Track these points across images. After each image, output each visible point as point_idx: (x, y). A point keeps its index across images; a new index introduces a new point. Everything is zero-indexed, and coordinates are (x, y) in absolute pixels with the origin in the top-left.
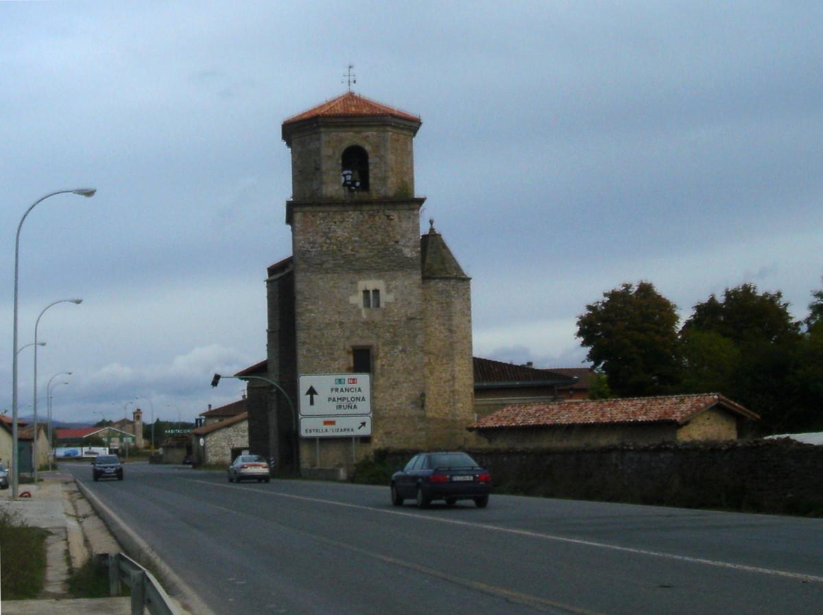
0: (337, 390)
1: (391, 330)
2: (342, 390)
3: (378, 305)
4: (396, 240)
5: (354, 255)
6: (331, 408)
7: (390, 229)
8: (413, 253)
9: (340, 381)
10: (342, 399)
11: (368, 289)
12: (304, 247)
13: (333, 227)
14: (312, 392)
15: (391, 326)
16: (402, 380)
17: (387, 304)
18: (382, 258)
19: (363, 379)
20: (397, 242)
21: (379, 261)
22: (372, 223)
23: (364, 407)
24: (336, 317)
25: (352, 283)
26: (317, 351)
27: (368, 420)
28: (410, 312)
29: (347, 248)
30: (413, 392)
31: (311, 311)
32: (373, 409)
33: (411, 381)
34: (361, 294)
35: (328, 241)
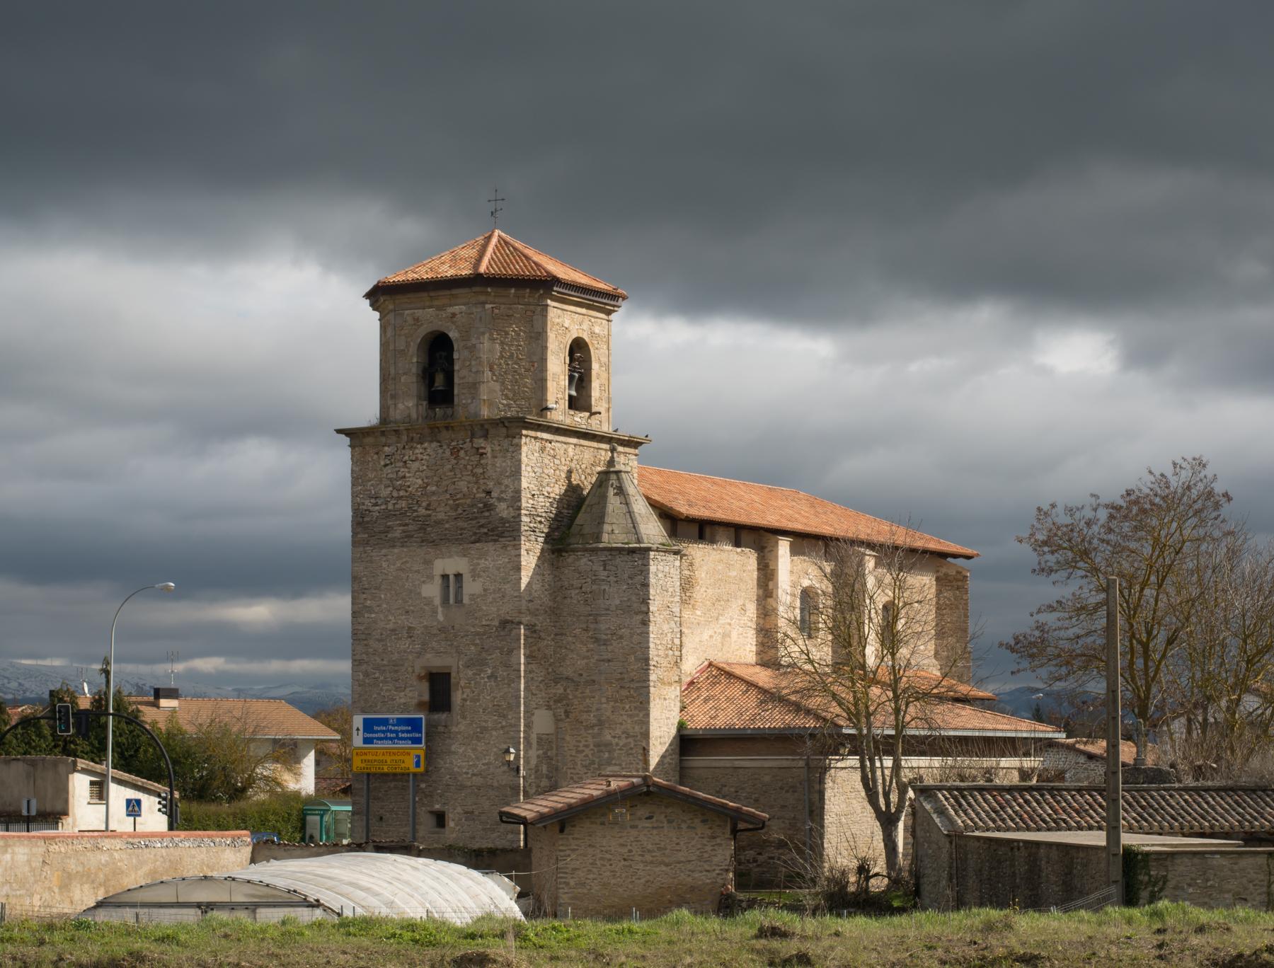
12: (363, 504)
17: (473, 597)
35: (395, 494)
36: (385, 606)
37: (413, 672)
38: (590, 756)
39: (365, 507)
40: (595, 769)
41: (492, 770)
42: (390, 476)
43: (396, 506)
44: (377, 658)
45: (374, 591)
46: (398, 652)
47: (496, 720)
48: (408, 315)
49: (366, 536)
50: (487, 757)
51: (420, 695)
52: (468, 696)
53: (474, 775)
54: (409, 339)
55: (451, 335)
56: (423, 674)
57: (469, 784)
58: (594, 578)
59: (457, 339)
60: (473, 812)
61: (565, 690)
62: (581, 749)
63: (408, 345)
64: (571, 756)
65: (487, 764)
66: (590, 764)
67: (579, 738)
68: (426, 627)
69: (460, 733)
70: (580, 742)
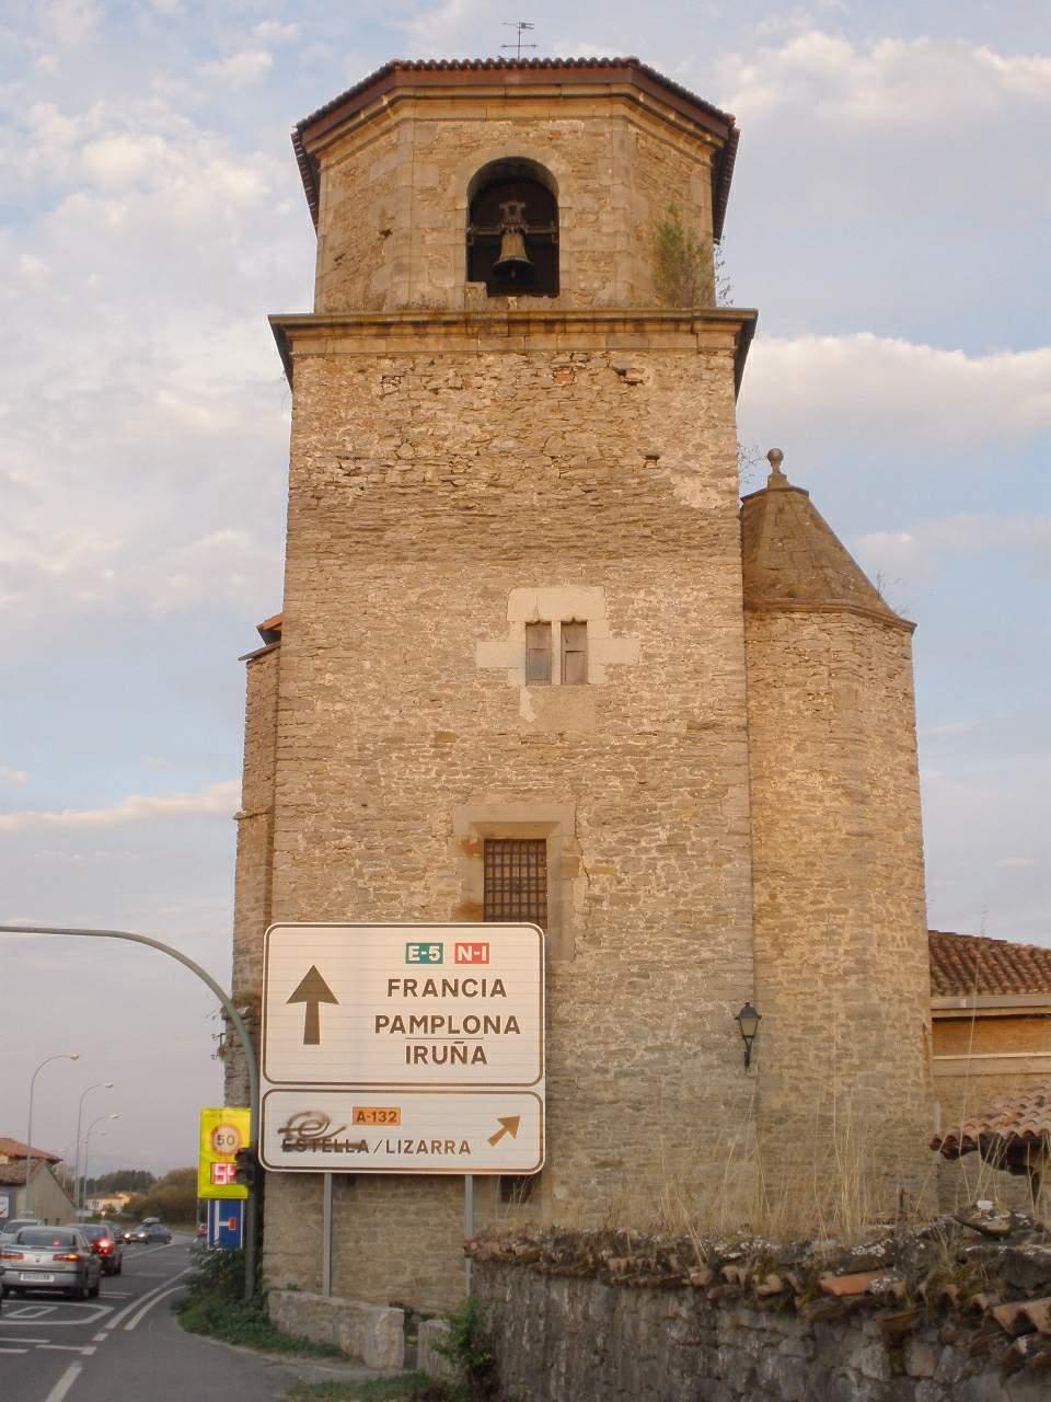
0: (410, 986)
2: (430, 988)
4: (650, 450)
5: (497, 498)
8: (712, 492)
9: (424, 954)
10: (434, 1023)
11: (545, 617)
12: (322, 471)
14: (313, 990)
15: (630, 751)
17: (615, 671)
18: (598, 508)
21: (592, 519)
24: (424, 719)
25: (487, 594)
26: (347, 840)
29: (475, 476)
31: (332, 693)
33: (702, 963)
34: (518, 635)
35: (406, 452)
36: (373, 685)
37: (451, 833)
38: (838, 1038)
39: (326, 478)
40: (852, 1067)
41: (673, 1063)
42: (394, 416)
43: (409, 476)
44: (348, 803)
45: (345, 654)
46: (407, 790)
47: (682, 947)
48: (444, 129)
49: (328, 535)
50: (661, 1033)
51: (467, 888)
52: (603, 890)
53: (621, 1074)
54: (447, 171)
55: (551, 166)
56: (475, 841)
57: (608, 1096)
58: (833, 665)
59: (563, 175)
60: (621, 1163)
61: (773, 897)
62: (815, 1023)
63: (444, 181)
64: (791, 1039)
65: (660, 1049)
66: (840, 1057)
67: (810, 1001)
68: (486, 735)
69: (583, 976)
70: (813, 1008)
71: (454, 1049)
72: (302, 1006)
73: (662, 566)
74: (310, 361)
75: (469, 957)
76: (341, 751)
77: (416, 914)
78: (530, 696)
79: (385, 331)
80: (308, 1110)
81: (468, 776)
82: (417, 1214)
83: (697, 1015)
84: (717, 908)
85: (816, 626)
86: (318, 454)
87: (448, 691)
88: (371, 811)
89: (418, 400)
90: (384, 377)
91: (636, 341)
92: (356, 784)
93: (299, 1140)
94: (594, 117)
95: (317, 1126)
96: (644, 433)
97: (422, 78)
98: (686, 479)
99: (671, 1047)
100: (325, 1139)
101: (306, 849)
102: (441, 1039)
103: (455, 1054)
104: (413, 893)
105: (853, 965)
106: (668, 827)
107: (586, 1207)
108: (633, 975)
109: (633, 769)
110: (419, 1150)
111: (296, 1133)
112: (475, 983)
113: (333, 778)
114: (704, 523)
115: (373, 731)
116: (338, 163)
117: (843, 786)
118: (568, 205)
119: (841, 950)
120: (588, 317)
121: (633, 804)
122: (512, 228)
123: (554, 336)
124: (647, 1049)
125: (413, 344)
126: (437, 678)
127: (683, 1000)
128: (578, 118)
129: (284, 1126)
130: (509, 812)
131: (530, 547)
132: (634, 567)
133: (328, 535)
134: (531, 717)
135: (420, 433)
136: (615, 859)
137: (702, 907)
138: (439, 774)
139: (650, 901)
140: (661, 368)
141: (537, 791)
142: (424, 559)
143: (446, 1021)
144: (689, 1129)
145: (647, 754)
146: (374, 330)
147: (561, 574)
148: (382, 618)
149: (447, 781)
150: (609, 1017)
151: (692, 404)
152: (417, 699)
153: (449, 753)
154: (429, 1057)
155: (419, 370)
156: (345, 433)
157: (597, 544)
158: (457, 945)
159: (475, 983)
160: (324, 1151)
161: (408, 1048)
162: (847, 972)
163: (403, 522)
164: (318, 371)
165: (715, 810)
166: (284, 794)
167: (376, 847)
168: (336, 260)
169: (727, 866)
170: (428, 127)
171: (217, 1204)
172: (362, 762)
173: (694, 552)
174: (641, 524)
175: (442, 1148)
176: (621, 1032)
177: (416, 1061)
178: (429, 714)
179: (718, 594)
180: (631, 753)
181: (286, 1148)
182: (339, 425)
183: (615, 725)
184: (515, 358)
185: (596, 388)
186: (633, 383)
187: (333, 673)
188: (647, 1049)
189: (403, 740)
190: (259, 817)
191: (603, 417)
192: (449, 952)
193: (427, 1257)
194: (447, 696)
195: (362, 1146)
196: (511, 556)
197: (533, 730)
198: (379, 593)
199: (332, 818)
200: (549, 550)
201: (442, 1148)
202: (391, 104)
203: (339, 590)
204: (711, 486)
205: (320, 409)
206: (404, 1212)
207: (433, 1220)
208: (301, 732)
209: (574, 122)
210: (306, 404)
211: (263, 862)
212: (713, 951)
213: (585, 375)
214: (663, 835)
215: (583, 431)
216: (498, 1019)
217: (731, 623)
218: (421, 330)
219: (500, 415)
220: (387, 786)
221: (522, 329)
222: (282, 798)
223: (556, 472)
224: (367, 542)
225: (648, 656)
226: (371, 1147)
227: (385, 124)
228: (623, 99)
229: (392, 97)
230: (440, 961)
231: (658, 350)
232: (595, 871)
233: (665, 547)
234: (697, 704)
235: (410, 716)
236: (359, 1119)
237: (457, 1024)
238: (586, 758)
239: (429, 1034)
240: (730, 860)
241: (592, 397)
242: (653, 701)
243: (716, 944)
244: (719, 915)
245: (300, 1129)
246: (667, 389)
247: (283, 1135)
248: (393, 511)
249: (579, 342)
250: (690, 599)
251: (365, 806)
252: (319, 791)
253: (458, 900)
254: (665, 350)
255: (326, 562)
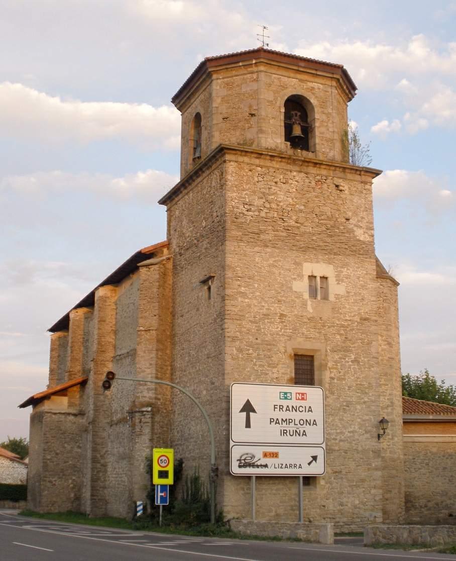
0: (281, 408)
1: (342, 332)
2: (288, 409)
3: (325, 297)
4: (347, 217)
5: (298, 228)
6: (273, 434)
7: (340, 202)
8: (366, 235)
9: (286, 396)
10: (288, 421)
11: (315, 275)
12: (238, 208)
13: (274, 188)
14: (248, 408)
15: (343, 326)
16: (354, 399)
17: (337, 296)
18: (331, 236)
19: (314, 395)
20: (348, 220)
21: (329, 240)
22: (320, 191)
23: (315, 434)
24: (276, 308)
25: (296, 263)
26: (251, 351)
27: (320, 453)
28: (366, 309)
29: (290, 218)
30: (367, 418)
31: (244, 295)
32: (326, 440)
33: (365, 402)
34: (306, 280)
35: (268, 205)
37: (286, 351)
41: (357, 437)
42: (263, 190)
43: (268, 215)
44: (251, 337)
47: (359, 396)
49: (241, 233)
52: (335, 375)
53: (341, 441)
59: (316, 105)
60: (341, 472)
63: (275, 99)
68: (296, 316)
71: (296, 431)
72: (245, 414)
73: (351, 260)
74: (232, 163)
75: (300, 398)
76: (248, 318)
77: (275, 381)
78: (311, 303)
79: (259, 156)
80: (247, 452)
81: (291, 331)
82: (276, 490)
83: (364, 421)
84: (369, 383)
85: (379, 284)
86: (236, 201)
87: (283, 298)
88: (259, 341)
89: (271, 186)
90: (259, 174)
91: (342, 175)
92: (253, 331)
93: (244, 464)
94: (325, 84)
95: (250, 458)
96: (345, 210)
97: (270, 56)
98: (359, 229)
99: (356, 432)
100: (253, 463)
101: (236, 354)
102: (291, 427)
103: (297, 433)
104: (273, 373)
105: (390, 404)
106: (354, 354)
107: (331, 487)
108: (344, 406)
109: (343, 332)
110: (285, 467)
111: (243, 461)
112: (302, 407)
113: (245, 328)
114: (364, 246)
115: (259, 311)
116: (223, 78)
117: (388, 341)
118: (318, 118)
119: (386, 398)
120: (330, 164)
121: (343, 345)
122: (298, 122)
123: (316, 168)
124: (349, 432)
125: (268, 163)
126: (280, 293)
127: (360, 415)
128: (322, 84)
129: (239, 459)
130: (305, 346)
131: (309, 248)
132: (343, 259)
133: (241, 233)
134: (311, 311)
135: (272, 198)
136: (338, 364)
137: (365, 383)
138: (281, 329)
139: (349, 380)
140: (350, 186)
141: (314, 338)
142: (275, 247)
143: (293, 421)
144: (361, 460)
145: (348, 328)
146: (255, 155)
147: (320, 259)
148: (261, 268)
149: (284, 332)
150: (337, 421)
151: (360, 201)
152: (273, 300)
153: (284, 322)
154: (288, 434)
155: (271, 174)
156: (246, 194)
157: (331, 249)
158: (296, 393)
159: (302, 407)
160: (253, 468)
161: (281, 430)
162: (388, 406)
163: (267, 232)
164: (235, 168)
165: (368, 349)
166: (228, 332)
167: (261, 355)
168: (224, 119)
169: (372, 369)
170: (270, 76)
171: (159, 486)
172: (255, 322)
173: (361, 256)
174: (344, 244)
175: (293, 467)
176: (340, 426)
177: (284, 435)
178: (277, 306)
179: (369, 272)
180: (343, 327)
181: (240, 467)
182: (243, 191)
183: (338, 316)
184: (303, 175)
185: (330, 191)
186: (341, 191)
187: (244, 287)
188: (349, 432)
189: (269, 315)
190: (151, 331)
191: (332, 202)
192: (294, 396)
193: (280, 506)
194: (284, 300)
195: (266, 466)
196: (305, 249)
197: (312, 316)
198: (260, 258)
199: (245, 343)
200: (316, 250)
201: (293, 467)
202: (256, 63)
203: (245, 256)
204: (367, 233)
205: (236, 183)
206: (272, 490)
207: (281, 493)
208: (233, 309)
209: (319, 85)
210: (231, 180)
211: (154, 349)
212: (368, 399)
213: (326, 185)
214: (353, 357)
215: (326, 206)
216: (310, 420)
217: (373, 283)
218: (272, 158)
219: (298, 196)
220: (264, 332)
221: (306, 164)
222: (228, 334)
223: (317, 220)
224: (254, 238)
225: (348, 292)
226: (269, 466)
227: (250, 69)
228: (336, 80)
229: (258, 61)
230: (291, 399)
231: (349, 180)
232: (333, 368)
233: (352, 253)
234: (363, 311)
235: (271, 306)
236: (265, 456)
237: (297, 422)
238: (329, 327)
239: (288, 426)
240: (373, 367)
241: (328, 194)
242: (350, 309)
243: (369, 396)
244: (370, 386)
245: (244, 460)
246: (352, 195)
247: (238, 462)
248: (263, 227)
249: (324, 172)
250: (360, 273)
251: (257, 339)
252: (241, 332)
253: (288, 376)
254: (351, 180)
255: (240, 244)
